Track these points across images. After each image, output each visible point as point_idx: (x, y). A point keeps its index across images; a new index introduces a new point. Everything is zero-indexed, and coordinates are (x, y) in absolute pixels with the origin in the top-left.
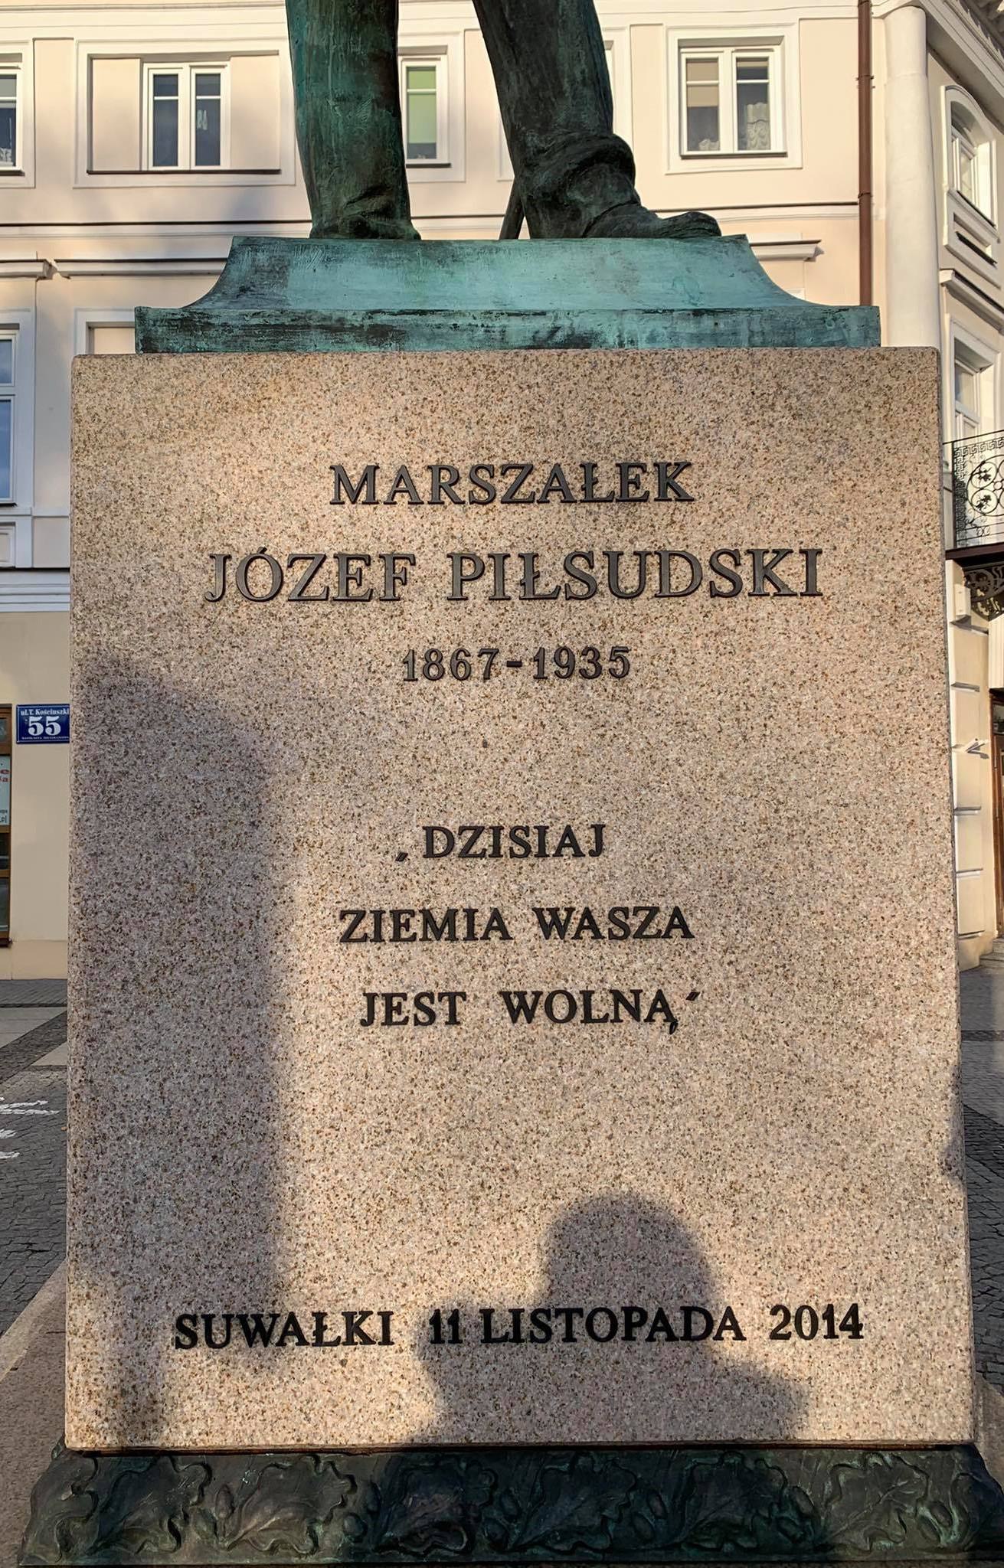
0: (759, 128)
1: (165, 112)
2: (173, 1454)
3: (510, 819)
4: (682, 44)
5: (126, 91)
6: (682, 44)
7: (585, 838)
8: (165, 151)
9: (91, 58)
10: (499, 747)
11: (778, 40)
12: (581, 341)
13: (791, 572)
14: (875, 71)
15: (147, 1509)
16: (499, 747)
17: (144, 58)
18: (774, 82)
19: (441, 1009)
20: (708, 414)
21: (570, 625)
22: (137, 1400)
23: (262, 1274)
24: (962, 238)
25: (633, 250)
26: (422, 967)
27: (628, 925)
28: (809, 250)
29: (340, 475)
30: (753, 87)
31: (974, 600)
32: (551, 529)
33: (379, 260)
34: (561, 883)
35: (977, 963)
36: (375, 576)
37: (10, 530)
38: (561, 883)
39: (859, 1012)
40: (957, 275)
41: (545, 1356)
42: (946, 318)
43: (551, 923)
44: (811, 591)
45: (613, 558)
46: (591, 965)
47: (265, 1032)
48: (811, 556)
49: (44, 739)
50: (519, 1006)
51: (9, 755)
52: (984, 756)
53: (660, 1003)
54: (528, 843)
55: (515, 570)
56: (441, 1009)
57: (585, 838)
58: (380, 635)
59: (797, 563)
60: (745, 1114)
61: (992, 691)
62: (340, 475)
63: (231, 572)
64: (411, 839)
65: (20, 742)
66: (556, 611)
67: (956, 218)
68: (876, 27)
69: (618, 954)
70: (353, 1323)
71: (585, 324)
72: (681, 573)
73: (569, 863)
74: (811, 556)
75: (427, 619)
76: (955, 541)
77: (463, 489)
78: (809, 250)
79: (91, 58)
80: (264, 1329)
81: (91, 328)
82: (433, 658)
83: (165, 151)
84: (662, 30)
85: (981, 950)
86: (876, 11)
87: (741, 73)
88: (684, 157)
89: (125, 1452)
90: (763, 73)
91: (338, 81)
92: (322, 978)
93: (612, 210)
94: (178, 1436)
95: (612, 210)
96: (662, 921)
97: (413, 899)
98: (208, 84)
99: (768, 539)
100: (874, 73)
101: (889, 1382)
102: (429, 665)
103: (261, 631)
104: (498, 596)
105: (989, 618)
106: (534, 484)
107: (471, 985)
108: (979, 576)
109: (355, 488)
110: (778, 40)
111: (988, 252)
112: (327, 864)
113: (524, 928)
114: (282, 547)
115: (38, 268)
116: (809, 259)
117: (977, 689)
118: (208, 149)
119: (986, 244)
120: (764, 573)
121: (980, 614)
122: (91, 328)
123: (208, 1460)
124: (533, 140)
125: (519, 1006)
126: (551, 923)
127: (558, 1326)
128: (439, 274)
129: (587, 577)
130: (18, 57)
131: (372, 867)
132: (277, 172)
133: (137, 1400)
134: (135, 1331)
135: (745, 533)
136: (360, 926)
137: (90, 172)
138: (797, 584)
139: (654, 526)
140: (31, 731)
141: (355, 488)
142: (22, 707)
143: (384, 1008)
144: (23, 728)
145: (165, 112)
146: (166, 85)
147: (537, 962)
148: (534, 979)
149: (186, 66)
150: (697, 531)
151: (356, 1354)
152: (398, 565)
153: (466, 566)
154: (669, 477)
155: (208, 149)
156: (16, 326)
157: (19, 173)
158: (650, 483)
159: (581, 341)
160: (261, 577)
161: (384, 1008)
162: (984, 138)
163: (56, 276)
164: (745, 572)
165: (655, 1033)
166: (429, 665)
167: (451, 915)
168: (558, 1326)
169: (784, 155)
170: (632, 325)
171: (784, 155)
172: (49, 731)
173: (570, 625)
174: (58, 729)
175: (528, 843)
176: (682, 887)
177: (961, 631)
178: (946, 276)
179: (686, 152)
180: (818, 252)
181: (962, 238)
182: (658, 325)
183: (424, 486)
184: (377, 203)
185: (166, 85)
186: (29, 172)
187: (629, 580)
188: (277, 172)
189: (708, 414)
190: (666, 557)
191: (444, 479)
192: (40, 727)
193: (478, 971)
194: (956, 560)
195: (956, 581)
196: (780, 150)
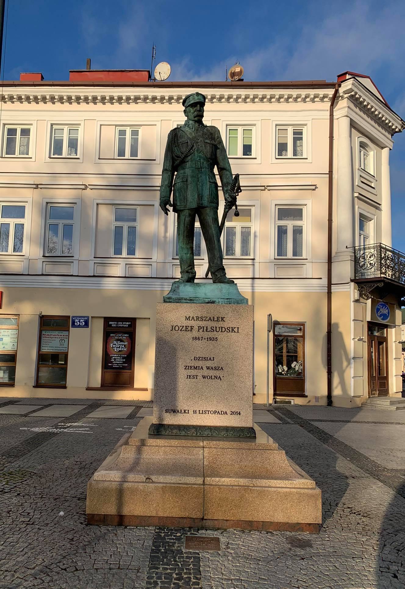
0: (300, 148)
1: (122, 142)
2: (165, 425)
3: (204, 356)
4: (276, 125)
5: (111, 136)
6: (276, 125)
7: (212, 359)
8: (121, 153)
9: (101, 125)
10: (201, 348)
11: (306, 125)
12: (213, 302)
13: (236, 330)
14: (334, 135)
15: (162, 429)
16: (201, 348)
17: (116, 126)
18: (304, 136)
19: (195, 377)
20: (227, 312)
21: (211, 335)
22: (160, 418)
23: (174, 405)
24: (362, 182)
25: (223, 285)
26: (193, 372)
27: (216, 369)
28: (314, 187)
29: (186, 317)
30: (298, 136)
31: (361, 295)
32: (210, 324)
33: (190, 286)
34: (209, 364)
35: (360, 405)
36: (189, 328)
37: (72, 264)
38: (209, 364)
39: (241, 379)
40: (360, 194)
41: (206, 415)
42: (356, 207)
43: (208, 368)
44: (238, 332)
45: (216, 327)
46: (212, 373)
47: (176, 379)
48: (238, 328)
49: (79, 326)
50: (204, 377)
51: (69, 331)
52: (365, 342)
53: (220, 377)
54: (205, 359)
55: (205, 328)
56: (195, 377)
57: (212, 359)
58: (189, 335)
59: (236, 329)
60: (228, 390)
61: (368, 322)
62: (186, 317)
63: (173, 328)
64: (193, 358)
65: (72, 327)
66: (210, 333)
67: (360, 176)
68: (335, 122)
69: (215, 372)
70: (185, 411)
71: (214, 300)
72: (224, 329)
73: (210, 361)
74: (238, 328)
75: (195, 333)
76: (355, 276)
77: (200, 319)
78: (314, 187)
79: (101, 125)
80: (175, 411)
81: (97, 204)
82: (196, 338)
83: (121, 153)
84: (271, 121)
85: (362, 401)
86: (335, 117)
87: (295, 133)
88: (276, 159)
89: (160, 424)
90: (301, 133)
91: (185, 251)
92: (182, 374)
93: (221, 276)
94: (165, 422)
95: (221, 276)
96: (220, 368)
97: (193, 365)
98: (135, 133)
99: (233, 326)
100: (334, 136)
101: (243, 420)
102: (195, 339)
103: (177, 335)
104: (203, 331)
105: (367, 300)
106: (208, 319)
107: (199, 374)
108: (362, 287)
109: (188, 319)
110: (306, 125)
111: (373, 186)
112: (183, 360)
113: (205, 368)
114: (179, 325)
115: (83, 187)
116: (313, 190)
117: (362, 321)
118: (134, 152)
119: (372, 182)
120: (233, 330)
121: (364, 298)
122: (97, 204)
123: (169, 426)
124: (211, 264)
125: (204, 377)
126: (208, 368)
127: (207, 412)
128: (198, 288)
129: (213, 330)
130: (80, 124)
131: (188, 361)
132: (155, 160)
133: (160, 418)
134: (160, 411)
135: (231, 325)
136: (186, 368)
137: (99, 159)
138: (236, 331)
139: (221, 324)
140: (76, 324)
141: (188, 319)
142: (73, 317)
143: (189, 377)
144: (73, 322)
145: (122, 142)
146: (122, 133)
147: (206, 372)
148: (206, 374)
149: (129, 128)
150: (225, 325)
151: (185, 414)
152: (192, 328)
153: (199, 328)
154: (222, 319)
155: (134, 152)
156: (76, 203)
157: (78, 159)
158: (220, 319)
159: (213, 302)
160: (177, 328)
161: (189, 377)
162: (372, 150)
163: (88, 189)
164: (231, 330)
165: (219, 380)
166: (195, 339)
167: (189, 317)
168: (207, 412)
169: (307, 159)
170: (220, 300)
171: (307, 159)
172: (81, 324)
173: (211, 335)
174: (84, 323)
175: (205, 359)
176: (222, 365)
177: (357, 304)
178: (356, 195)
179: (277, 157)
180: (316, 188)
181: (362, 182)
182: (222, 300)
183: (195, 319)
184: (190, 268)
185: (122, 133)
186: (81, 158)
187: (218, 330)
188: (155, 160)
189: (227, 312)
190: (222, 328)
191: (198, 318)
192: (78, 323)
193: (200, 373)
194: (355, 283)
195: (355, 289)
196: (306, 157)
